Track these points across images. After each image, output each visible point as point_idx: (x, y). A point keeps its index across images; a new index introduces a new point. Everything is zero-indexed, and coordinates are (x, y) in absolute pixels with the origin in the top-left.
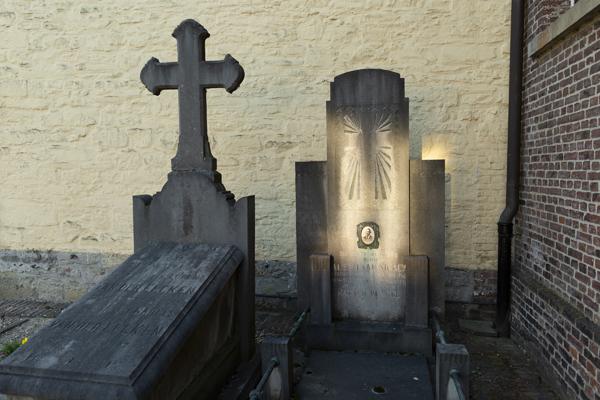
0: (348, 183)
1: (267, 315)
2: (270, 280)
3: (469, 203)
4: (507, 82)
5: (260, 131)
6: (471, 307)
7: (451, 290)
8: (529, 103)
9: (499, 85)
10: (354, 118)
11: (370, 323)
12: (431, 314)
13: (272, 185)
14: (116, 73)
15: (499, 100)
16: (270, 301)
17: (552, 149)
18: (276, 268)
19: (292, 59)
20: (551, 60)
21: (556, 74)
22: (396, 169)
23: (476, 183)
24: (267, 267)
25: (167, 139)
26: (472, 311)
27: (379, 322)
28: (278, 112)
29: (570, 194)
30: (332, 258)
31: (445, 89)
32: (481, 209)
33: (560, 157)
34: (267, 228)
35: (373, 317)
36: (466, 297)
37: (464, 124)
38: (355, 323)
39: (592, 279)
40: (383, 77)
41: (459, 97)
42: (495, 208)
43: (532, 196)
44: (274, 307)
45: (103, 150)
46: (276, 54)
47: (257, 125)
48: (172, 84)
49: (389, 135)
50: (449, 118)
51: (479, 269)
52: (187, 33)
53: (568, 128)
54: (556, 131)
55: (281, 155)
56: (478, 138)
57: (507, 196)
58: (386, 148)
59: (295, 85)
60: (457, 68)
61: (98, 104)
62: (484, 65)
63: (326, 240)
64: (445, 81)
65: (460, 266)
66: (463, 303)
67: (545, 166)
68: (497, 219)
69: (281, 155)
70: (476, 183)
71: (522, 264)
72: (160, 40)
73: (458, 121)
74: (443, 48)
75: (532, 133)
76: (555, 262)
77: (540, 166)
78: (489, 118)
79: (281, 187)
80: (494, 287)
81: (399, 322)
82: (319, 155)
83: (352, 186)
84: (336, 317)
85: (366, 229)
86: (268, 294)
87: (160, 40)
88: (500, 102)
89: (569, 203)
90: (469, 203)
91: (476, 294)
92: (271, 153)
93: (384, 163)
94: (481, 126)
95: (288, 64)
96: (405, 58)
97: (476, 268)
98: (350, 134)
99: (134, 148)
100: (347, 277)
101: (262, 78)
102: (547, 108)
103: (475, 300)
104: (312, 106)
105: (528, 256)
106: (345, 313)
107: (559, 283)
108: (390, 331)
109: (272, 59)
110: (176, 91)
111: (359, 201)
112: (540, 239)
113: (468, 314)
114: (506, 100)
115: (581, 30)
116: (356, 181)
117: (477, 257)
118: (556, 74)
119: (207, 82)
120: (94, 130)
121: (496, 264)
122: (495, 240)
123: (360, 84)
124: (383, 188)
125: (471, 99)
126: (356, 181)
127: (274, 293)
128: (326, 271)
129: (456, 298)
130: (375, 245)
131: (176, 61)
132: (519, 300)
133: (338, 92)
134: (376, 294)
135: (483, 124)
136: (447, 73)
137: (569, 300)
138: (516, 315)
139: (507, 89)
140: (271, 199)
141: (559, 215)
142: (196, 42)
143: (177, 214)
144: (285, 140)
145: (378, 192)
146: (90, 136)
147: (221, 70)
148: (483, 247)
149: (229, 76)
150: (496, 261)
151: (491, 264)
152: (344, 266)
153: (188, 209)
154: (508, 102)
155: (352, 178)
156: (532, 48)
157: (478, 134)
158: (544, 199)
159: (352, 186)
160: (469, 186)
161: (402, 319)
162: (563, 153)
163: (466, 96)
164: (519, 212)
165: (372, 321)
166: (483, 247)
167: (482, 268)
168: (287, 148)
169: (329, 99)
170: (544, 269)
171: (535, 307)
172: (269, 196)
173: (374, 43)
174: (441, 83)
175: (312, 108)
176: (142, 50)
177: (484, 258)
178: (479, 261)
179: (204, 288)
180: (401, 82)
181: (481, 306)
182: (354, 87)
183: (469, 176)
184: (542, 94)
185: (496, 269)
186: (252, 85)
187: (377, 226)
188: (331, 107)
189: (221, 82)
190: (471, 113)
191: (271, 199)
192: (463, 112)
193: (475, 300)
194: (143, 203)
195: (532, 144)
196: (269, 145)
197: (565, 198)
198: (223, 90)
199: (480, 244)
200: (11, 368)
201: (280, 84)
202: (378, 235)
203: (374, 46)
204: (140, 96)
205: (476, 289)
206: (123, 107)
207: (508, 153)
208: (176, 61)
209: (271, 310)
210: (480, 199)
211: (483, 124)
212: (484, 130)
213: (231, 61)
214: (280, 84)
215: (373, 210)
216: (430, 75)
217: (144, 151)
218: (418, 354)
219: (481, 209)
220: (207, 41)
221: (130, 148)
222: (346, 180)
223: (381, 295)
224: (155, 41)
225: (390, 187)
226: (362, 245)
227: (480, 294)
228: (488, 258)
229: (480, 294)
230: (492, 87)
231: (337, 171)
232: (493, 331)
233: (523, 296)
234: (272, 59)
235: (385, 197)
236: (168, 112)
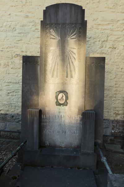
0: (51, 68)
1: (11, 142)
2: (14, 123)
3: (111, 88)
5: (12, 49)
6: (110, 138)
10: (56, 31)
11: (61, 149)
12: (96, 144)
13: (17, 76)
16: (14, 134)
18: (17, 118)
19: (30, 15)
22: (78, 61)
24: (13, 117)
26: (111, 140)
27: (67, 149)
28: (21, 40)
30: (41, 112)
32: (116, 91)
34: (14, 97)
35: (63, 145)
36: (108, 133)
38: (53, 148)
40: (73, 8)
41: (108, 36)
44: (16, 137)
46: (21, 11)
47: (10, 46)
49: (76, 41)
50: (103, 47)
56: (116, 57)
58: (74, 48)
59: (30, 27)
62: (120, 22)
63: (38, 101)
64: (102, 29)
66: (107, 136)
73: (107, 48)
81: (77, 149)
82: (34, 51)
84: (42, 145)
85: (60, 96)
86: (13, 131)
90: (111, 88)
91: (113, 131)
93: (72, 57)
94: (117, 51)
95: (27, 17)
97: (113, 119)
98: (53, 40)
100: (50, 122)
101: (14, 23)
103: (112, 134)
106: (47, 143)
108: (72, 155)
111: (57, 79)
113: (109, 141)
116: (56, 66)
117: (114, 114)
123: (60, 11)
124: (71, 71)
125: (114, 38)
126: (56, 67)
127: (16, 130)
128: (36, 119)
130: (65, 104)
134: (65, 132)
135: (119, 50)
140: (16, 83)
145: (66, 74)
152: (47, 116)
157: (116, 55)
161: (79, 147)
163: (111, 37)
165: (62, 148)
167: (116, 119)
169: (42, 20)
172: (15, 81)
174: (100, 30)
177: (117, 114)
178: (115, 115)
179: (43, 132)
180: (83, 11)
182: (56, 13)
183: (111, 75)
186: (9, 26)
187: (67, 93)
188: (44, 24)
190: (113, 44)
191: (16, 83)
192: (109, 44)
193: (112, 134)
196: (16, 56)
199: (116, 108)
201: (23, 26)
202: (67, 98)
205: (113, 129)
209: (14, 139)
211: (119, 50)
212: (118, 53)
214: (23, 26)
215: (64, 84)
216: (95, 26)
218: (88, 169)
219: (116, 91)
222: (50, 66)
223: (68, 133)
225: (75, 70)
226: (58, 104)
227: (115, 132)
228: (119, 114)
229: (115, 132)
231: (46, 61)
235: (72, 77)
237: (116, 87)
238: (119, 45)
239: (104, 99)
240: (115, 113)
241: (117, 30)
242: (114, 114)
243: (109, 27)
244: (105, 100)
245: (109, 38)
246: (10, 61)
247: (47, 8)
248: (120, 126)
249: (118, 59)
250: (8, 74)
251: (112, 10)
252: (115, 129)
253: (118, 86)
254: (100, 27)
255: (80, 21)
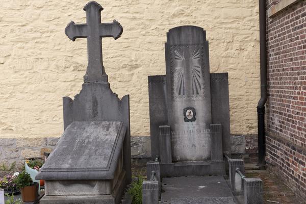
0: (178, 86)
4: (259, 29)
7: (233, 147)
8: (270, 41)
9: (255, 30)
14: (24, 24)
15: (255, 38)
17: (280, 66)
20: (278, 21)
21: (280, 28)
23: (244, 86)
25: (58, 64)
28: (129, 47)
29: (288, 88)
31: (225, 33)
32: (248, 100)
33: (283, 70)
37: (237, 52)
39: (296, 126)
40: (195, 31)
42: (255, 99)
43: (273, 91)
45: (16, 72)
46: (127, 12)
47: (116, 54)
48: (84, 35)
51: (248, 134)
52: (92, 9)
53: (285, 56)
54: (282, 57)
55: (131, 72)
56: (244, 60)
57: (261, 92)
59: (139, 30)
60: (232, 20)
61: (12, 43)
64: (225, 28)
65: (238, 133)
66: (240, 154)
67: (278, 75)
68: (257, 105)
69: (131, 72)
70: (244, 86)
71: (271, 128)
72: (53, 3)
74: (223, 9)
75: (272, 57)
76: (283, 123)
77: (276, 75)
78: (250, 49)
79: (132, 92)
80: (257, 144)
83: (180, 88)
84: (174, 160)
87: (53, 3)
88: (255, 40)
89: (288, 92)
91: (247, 148)
92: (125, 72)
94: (246, 53)
96: (202, 15)
97: (246, 134)
99: (37, 70)
102: (277, 45)
104: (150, 42)
105: (273, 123)
106: (179, 158)
107: (285, 132)
109: (124, 15)
110: (86, 39)
112: (277, 112)
114: (258, 39)
115: (293, 8)
117: (247, 127)
118: (277, 34)
119: (104, 35)
120: (9, 60)
121: (257, 131)
122: (256, 117)
123: (182, 33)
125: (240, 38)
126: (182, 85)
129: (236, 152)
131: (86, 23)
132: (269, 147)
133: (171, 39)
134: (195, 146)
136: (226, 23)
137: (289, 139)
138: (268, 156)
139: (259, 32)
141: (284, 99)
142: (97, 13)
143: (88, 106)
144: (134, 63)
146: (7, 63)
147: (112, 28)
148: (250, 121)
149: (115, 31)
150: (257, 129)
151: (255, 131)
153: (95, 103)
154: (259, 40)
155: (180, 83)
156: (270, 13)
158: (278, 92)
159: (180, 88)
160: (241, 87)
161: (209, 159)
162: (285, 68)
164: (267, 101)
166: (250, 121)
167: (250, 133)
168: (135, 68)
170: (280, 128)
171: (276, 148)
173: (184, 6)
175: (150, 44)
176: (42, 9)
177: (251, 128)
178: (248, 129)
181: (251, 155)
182: (179, 35)
184: (275, 38)
185: (257, 133)
187: (194, 109)
189: (112, 35)
194: (68, 103)
195: (272, 63)
197: (286, 90)
198: (112, 39)
200: (50, 169)
202: (195, 114)
203: (184, 8)
204: (40, 38)
205: (247, 145)
206: (29, 45)
207: (261, 68)
208: (86, 23)
210: (247, 94)
213: (116, 24)
217: (44, 72)
220: (102, 12)
221: (34, 70)
224: (50, 4)
227: (250, 149)
228: (253, 128)
229: (250, 149)
230: (251, 32)
232: (258, 167)
233: (271, 143)
234: (124, 15)
236: (59, 48)
237: (247, 96)
238: (247, 45)
239: (148, 104)
240: (248, 126)
241: (243, 28)
242: (247, 127)
243: (234, 25)
244: (146, 103)
245: (235, 38)
246: (117, 72)
247: (170, 30)
248: (255, 141)
249: (246, 62)
250: (116, 88)
251: (235, 5)
252: (249, 145)
253: (249, 93)
254: (224, 26)
255: (202, 42)
